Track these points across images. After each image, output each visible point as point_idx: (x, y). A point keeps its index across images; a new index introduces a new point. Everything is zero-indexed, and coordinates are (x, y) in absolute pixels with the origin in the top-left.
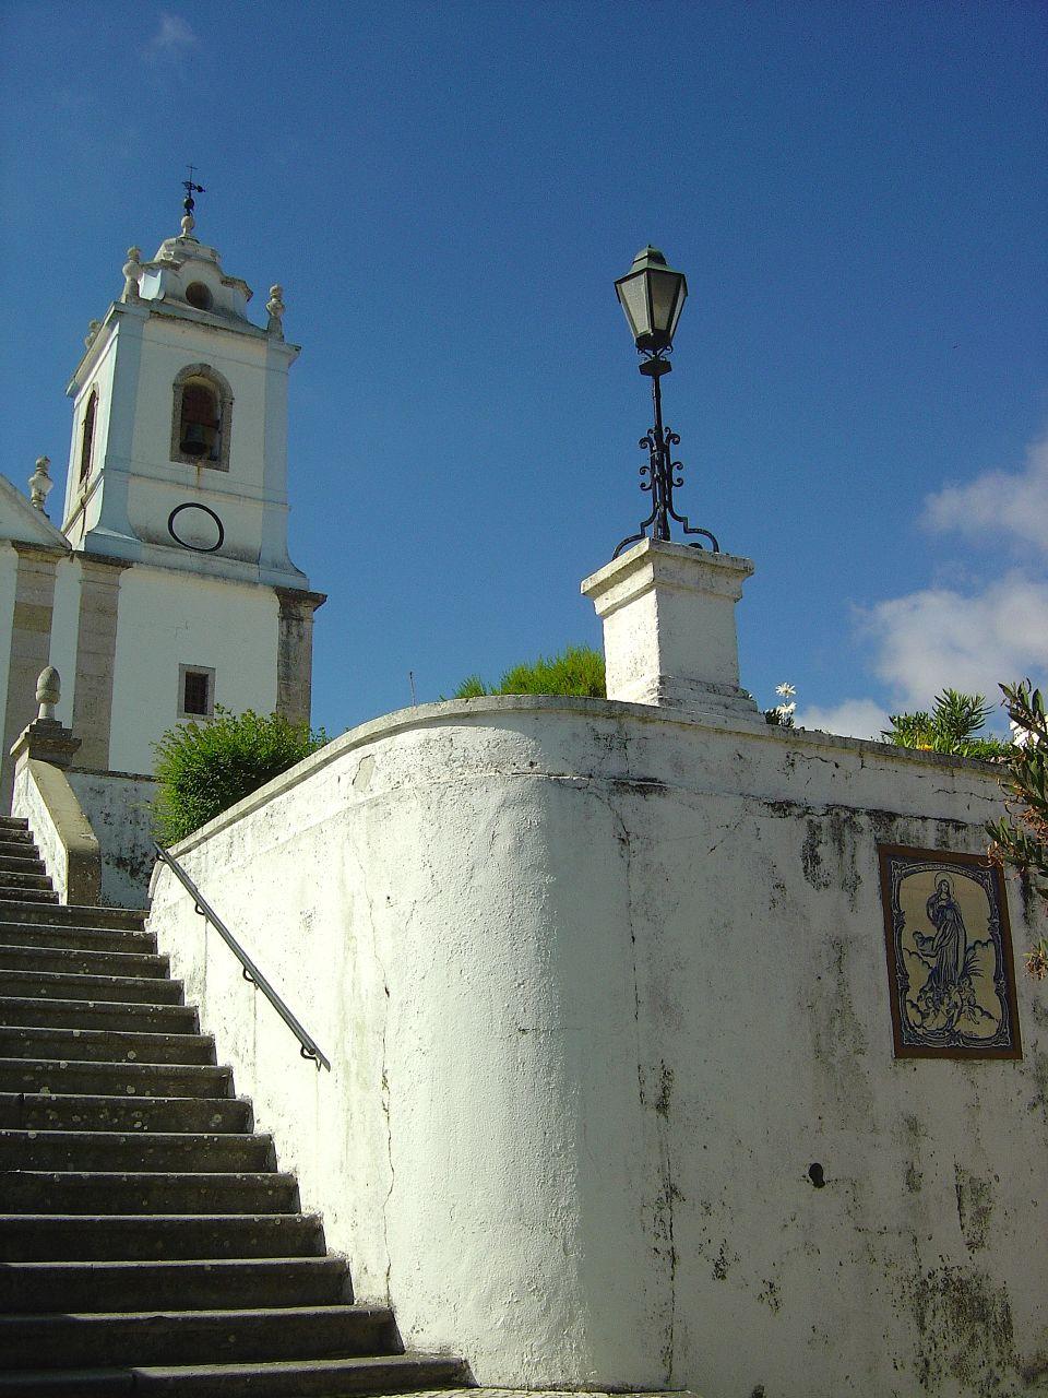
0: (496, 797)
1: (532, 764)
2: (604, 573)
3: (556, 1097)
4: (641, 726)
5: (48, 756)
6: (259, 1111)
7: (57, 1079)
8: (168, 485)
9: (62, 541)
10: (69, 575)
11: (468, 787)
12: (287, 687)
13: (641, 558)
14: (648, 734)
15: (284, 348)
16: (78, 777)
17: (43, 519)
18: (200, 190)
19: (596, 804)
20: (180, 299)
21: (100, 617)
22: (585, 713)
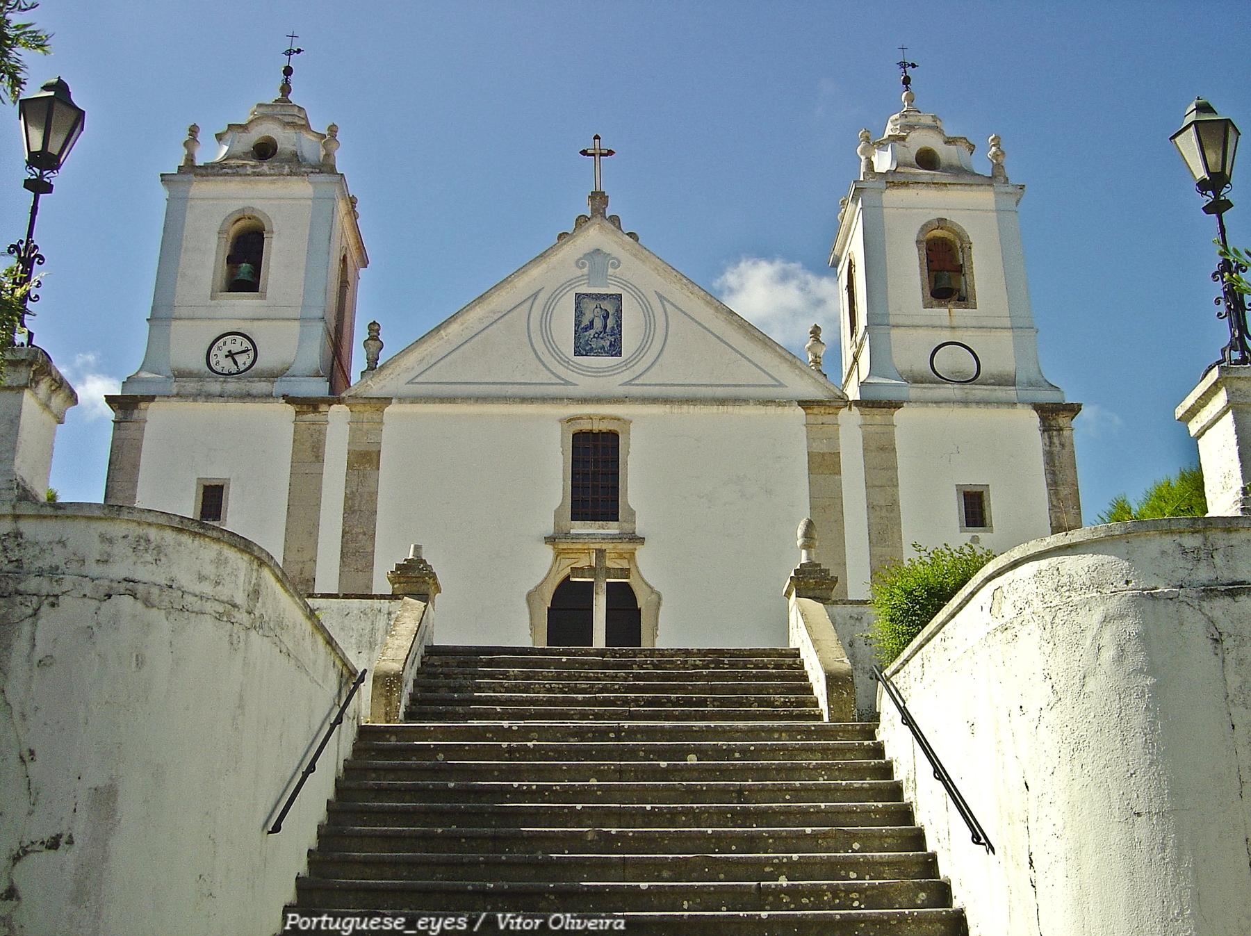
0: (1098, 614)
1: (1127, 582)
2: (1190, 401)
3: (1170, 870)
4: (1225, 535)
5: (810, 594)
6: (955, 891)
7: (792, 870)
8: (923, 329)
9: (839, 394)
10: (850, 423)
11: (1075, 608)
12: (1056, 493)
13: (1215, 384)
14: (1234, 542)
15: (1010, 189)
16: (838, 609)
17: (821, 379)
18: (914, 66)
19: (1187, 611)
20: (911, 166)
21: (881, 453)
22: (1171, 532)
